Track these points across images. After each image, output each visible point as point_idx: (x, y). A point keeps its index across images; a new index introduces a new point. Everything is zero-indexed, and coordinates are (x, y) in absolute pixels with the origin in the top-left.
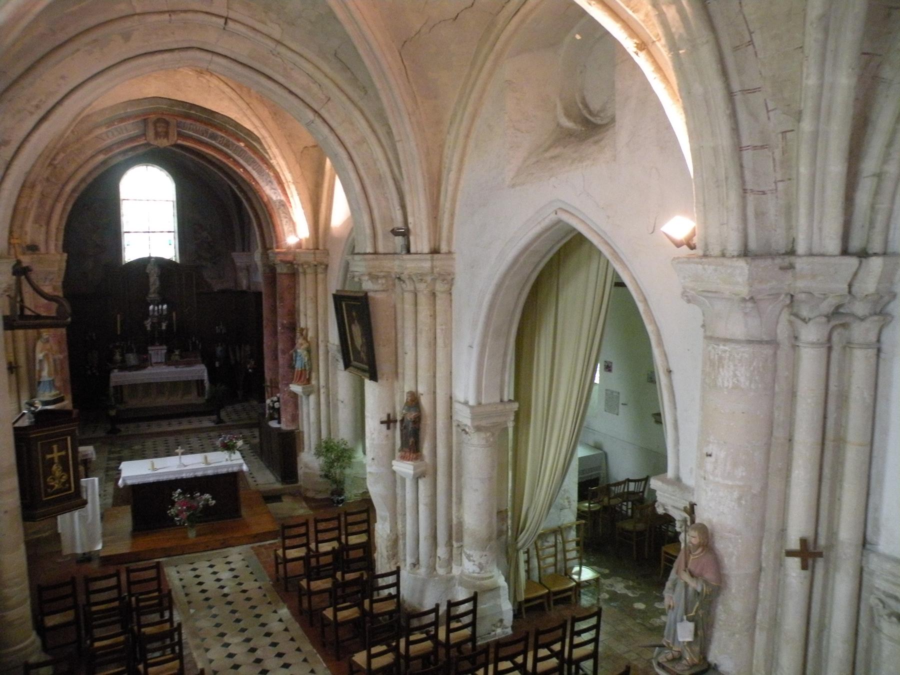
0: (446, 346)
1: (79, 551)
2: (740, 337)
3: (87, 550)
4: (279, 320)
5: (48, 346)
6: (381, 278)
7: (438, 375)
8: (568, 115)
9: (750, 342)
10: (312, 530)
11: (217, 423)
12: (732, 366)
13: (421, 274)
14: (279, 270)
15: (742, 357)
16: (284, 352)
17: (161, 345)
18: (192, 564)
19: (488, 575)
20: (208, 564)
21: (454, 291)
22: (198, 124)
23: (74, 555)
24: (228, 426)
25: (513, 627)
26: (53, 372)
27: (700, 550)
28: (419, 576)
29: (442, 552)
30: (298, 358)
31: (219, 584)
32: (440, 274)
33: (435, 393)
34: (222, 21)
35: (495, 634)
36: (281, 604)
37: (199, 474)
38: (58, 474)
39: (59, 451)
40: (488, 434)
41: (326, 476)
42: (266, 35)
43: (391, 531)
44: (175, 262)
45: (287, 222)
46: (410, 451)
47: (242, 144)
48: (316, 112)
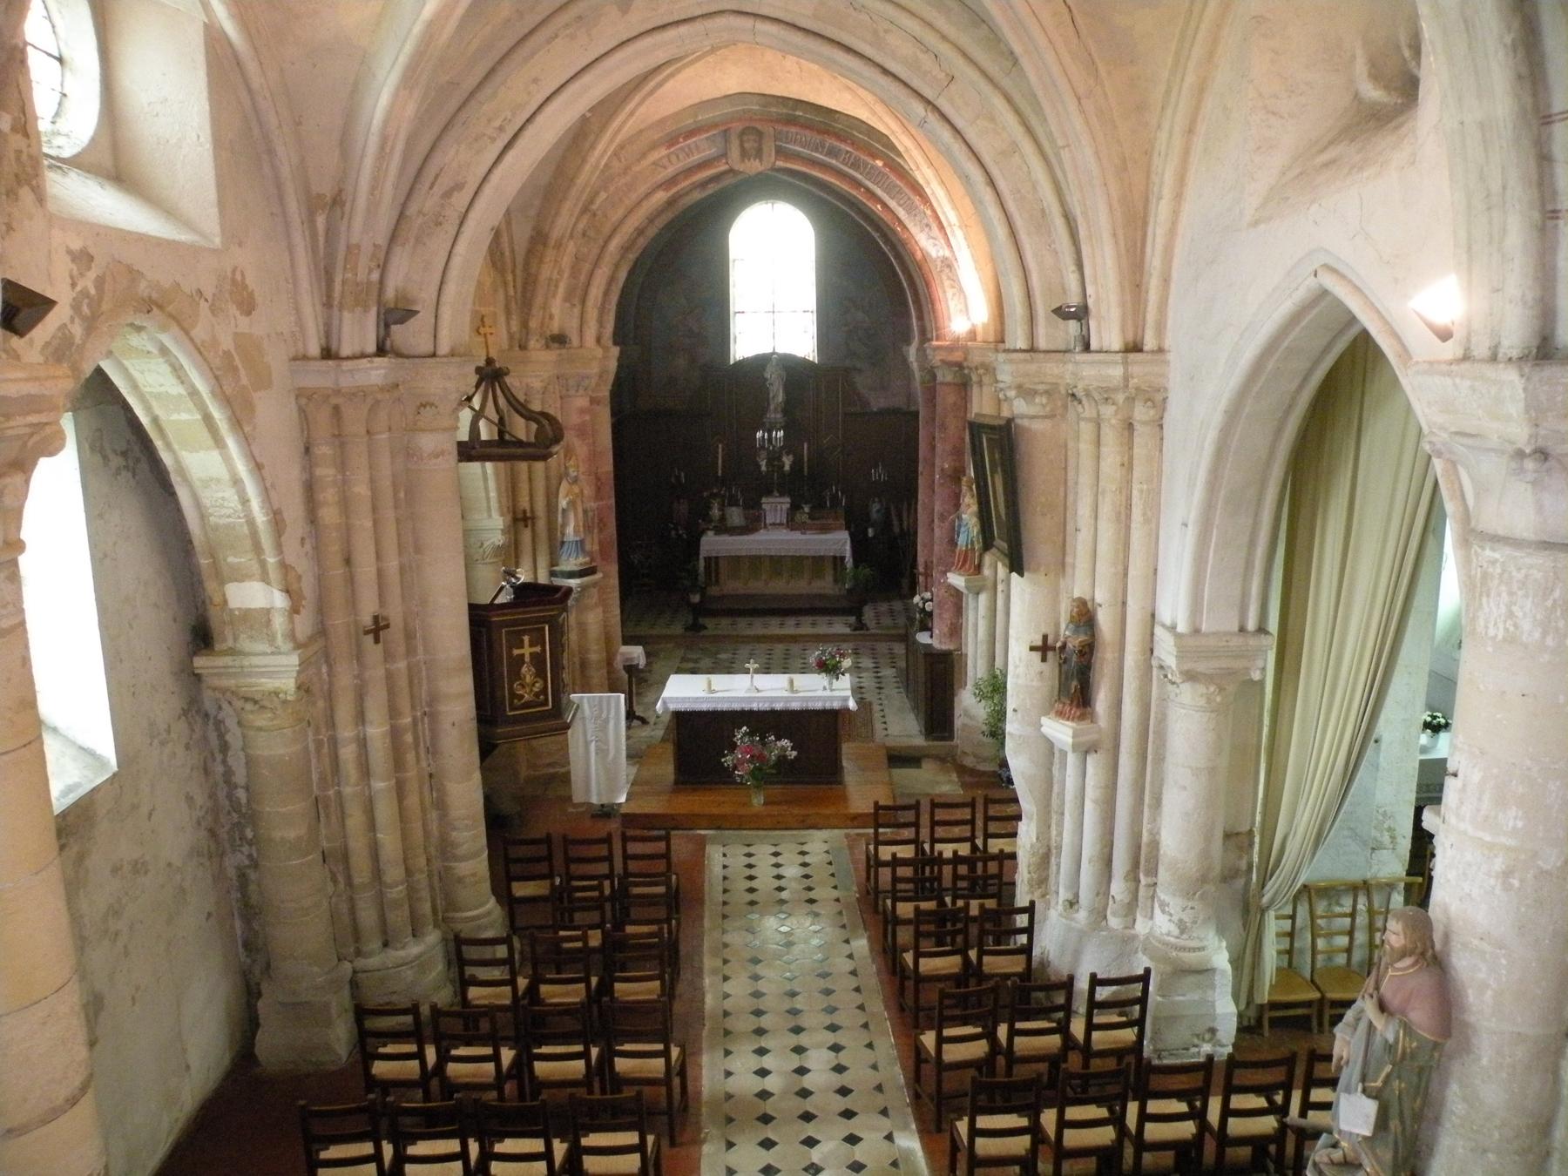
0: (1147, 521)
1: (594, 800)
2: (1525, 535)
3: (605, 801)
4: (938, 462)
5: (576, 489)
7: (1131, 573)
8: (1376, 76)
9: (1546, 545)
10: (925, 819)
11: (855, 629)
12: (1504, 595)
13: (1107, 390)
14: (940, 378)
15: (1526, 576)
16: (943, 518)
17: (782, 495)
20: (773, 849)
22: (807, 132)
24: (873, 635)
25: (1234, 1046)
27: (1408, 961)
28: (1073, 924)
29: (1118, 888)
30: (963, 529)
31: (777, 883)
32: (1138, 389)
33: (1124, 603)
35: (1199, 1053)
36: (861, 931)
37: (779, 706)
38: (528, 679)
39: (531, 645)
40: (1212, 689)
44: (813, 363)
45: (954, 294)
47: (879, 163)
48: (928, 102)
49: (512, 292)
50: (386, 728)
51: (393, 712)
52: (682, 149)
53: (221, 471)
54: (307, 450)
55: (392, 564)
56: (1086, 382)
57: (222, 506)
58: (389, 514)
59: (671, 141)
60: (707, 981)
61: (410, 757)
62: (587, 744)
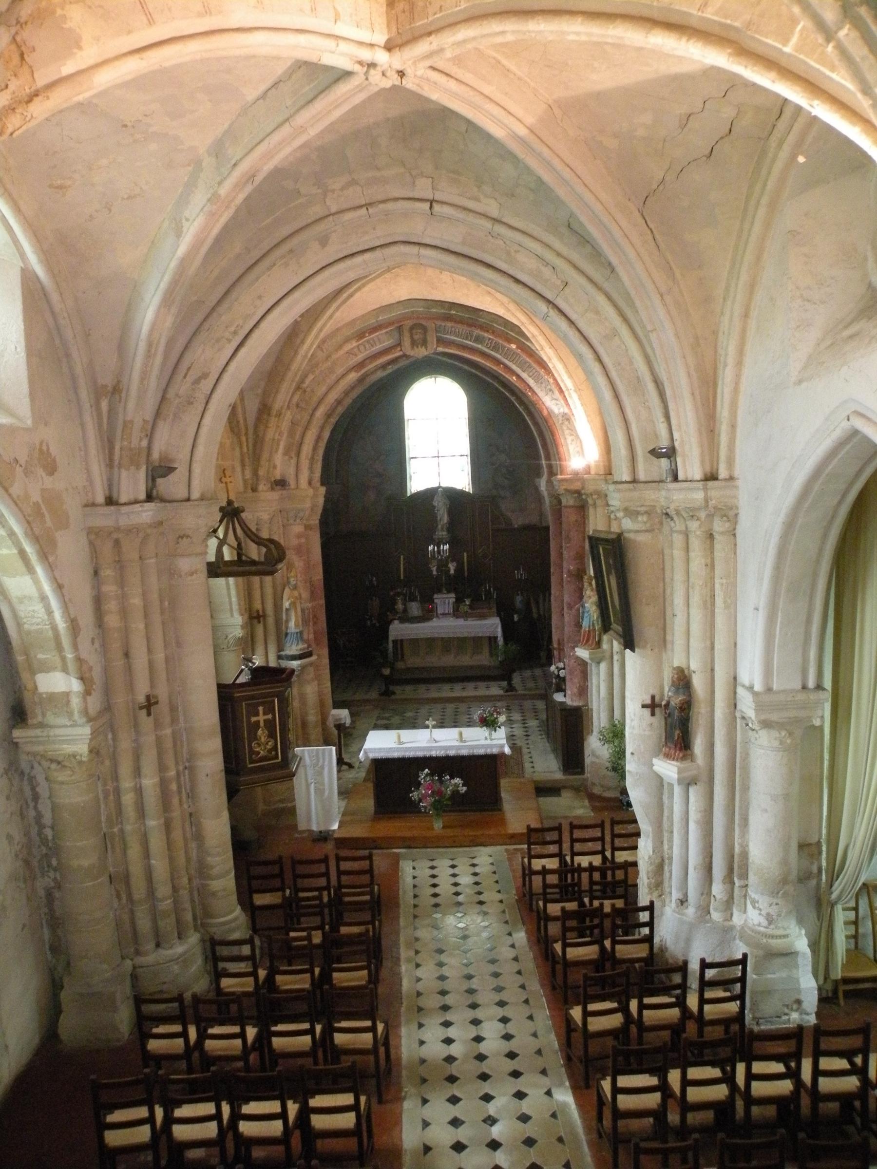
0: (727, 607)
1: (315, 828)
3: (322, 828)
4: (565, 565)
5: (296, 593)
6: (642, 514)
11: (507, 691)
13: (694, 509)
16: (570, 607)
17: (449, 592)
18: (432, 860)
19: (780, 932)
20: (451, 863)
21: (739, 531)
23: (310, 831)
25: (818, 1014)
26: (300, 623)
28: (685, 918)
29: (718, 889)
30: (586, 615)
31: (454, 889)
33: (712, 670)
34: (427, 206)
36: (520, 926)
37: (452, 753)
38: (263, 739)
39: (264, 714)
41: (614, 769)
42: (480, 214)
43: (654, 851)
44: (468, 493)
46: (676, 746)
47: (514, 346)
48: (549, 302)
49: (245, 450)
50: (156, 780)
51: (162, 768)
52: (368, 341)
53: (32, 591)
54: (96, 573)
55: (160, 656)
56: (677, 504)
57: (33, 617)
58: (156, 618)
59: (360, 335)
60: (403, 968)
61: (175, 801)
62: (308, 786)
